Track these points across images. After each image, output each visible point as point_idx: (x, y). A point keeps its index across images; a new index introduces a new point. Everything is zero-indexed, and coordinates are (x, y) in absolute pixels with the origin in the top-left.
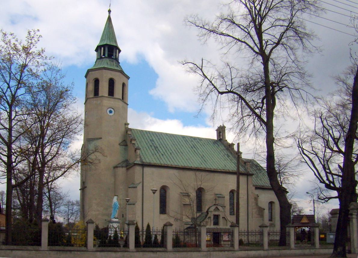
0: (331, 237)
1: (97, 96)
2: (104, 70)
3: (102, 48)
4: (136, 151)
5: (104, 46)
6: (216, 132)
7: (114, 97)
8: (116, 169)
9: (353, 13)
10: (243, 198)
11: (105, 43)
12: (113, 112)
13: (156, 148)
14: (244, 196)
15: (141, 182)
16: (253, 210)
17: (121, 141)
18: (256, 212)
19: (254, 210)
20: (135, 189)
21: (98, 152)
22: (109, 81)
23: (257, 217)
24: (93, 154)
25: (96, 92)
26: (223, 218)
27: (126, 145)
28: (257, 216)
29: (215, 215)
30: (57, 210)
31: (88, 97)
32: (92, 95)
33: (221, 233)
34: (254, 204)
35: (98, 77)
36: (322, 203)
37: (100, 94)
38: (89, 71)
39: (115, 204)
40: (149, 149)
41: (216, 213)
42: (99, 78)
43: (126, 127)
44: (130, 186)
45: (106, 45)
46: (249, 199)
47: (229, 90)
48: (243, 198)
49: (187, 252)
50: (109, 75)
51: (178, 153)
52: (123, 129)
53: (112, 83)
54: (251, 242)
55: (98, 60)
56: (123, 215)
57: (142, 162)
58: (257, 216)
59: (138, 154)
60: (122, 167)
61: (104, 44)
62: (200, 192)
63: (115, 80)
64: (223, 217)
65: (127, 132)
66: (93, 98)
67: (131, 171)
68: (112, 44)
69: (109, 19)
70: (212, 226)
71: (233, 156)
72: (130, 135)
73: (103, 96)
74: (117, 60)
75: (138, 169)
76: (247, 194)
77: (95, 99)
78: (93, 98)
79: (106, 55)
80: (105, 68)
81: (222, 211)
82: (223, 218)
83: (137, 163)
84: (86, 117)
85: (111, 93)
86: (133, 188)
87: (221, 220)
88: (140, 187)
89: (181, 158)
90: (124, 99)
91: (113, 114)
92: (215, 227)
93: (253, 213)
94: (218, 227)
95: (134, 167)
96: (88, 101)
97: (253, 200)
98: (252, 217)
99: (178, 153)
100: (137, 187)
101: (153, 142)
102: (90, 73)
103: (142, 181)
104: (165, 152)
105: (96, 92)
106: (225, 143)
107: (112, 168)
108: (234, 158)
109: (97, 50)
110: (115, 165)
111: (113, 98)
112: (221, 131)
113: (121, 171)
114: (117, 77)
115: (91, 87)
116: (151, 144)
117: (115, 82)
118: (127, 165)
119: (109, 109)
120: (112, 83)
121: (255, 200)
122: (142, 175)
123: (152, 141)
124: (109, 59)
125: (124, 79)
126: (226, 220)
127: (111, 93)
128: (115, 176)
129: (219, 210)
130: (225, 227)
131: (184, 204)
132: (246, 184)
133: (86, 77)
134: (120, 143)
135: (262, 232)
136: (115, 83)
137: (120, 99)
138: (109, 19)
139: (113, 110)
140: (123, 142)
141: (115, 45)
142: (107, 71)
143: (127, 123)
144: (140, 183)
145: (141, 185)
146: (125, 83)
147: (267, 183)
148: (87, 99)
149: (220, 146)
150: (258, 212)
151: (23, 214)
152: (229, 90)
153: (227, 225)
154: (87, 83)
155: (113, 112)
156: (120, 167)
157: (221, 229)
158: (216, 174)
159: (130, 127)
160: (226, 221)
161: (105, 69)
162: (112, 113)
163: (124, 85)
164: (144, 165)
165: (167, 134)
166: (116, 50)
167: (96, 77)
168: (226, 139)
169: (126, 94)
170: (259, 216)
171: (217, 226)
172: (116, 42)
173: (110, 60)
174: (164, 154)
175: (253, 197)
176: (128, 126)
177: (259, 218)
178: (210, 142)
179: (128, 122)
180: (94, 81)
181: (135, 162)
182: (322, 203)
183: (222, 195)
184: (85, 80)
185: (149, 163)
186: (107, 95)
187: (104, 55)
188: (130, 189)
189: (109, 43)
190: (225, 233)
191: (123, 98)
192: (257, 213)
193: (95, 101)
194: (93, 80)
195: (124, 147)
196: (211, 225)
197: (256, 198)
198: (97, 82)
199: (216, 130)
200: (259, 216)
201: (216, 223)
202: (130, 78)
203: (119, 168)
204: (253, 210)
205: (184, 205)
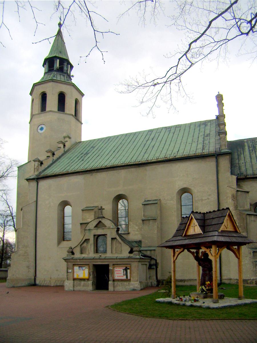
1: (45, 112)
7: (65, 112)
9: (202, 8)
10: (208, 199)
12: (43, 126)
29: (97, 237)
30: (245, 173)
31: (33, 113)
36: (226, 20)
37: (48, 109)
38: (35, 85)
41: (100, 232)
47: (186, 250)
49: (231, 168)
53: (62, 97)
54: (227, 282)
63: (66, 94)
69: (59, 33)
74: (69, 77)
76: (216, 191)
78: (39, 114)
81: (112, 227)
82: (112, 239)
90: (77, 116)
92: (97, 256)
102: (36, 87)
115: (38, 102)
119: (40, 131)
120: (62, 97)
125: (77, 95)
129: (106, 226)
133: (31, 94)
135: (24, 7)
137: (72, 115)
138: (59, 33)
141: (66, 58)
146: (78, 99)
148: (32, 116)
152: (186, 250)
163: (77, 102)
167: (42, 91)
172: (66, 53)
182: (226, 20)
184: (30, 98)
186: (56, 109)
191: (77, 114)
194: (40, 95)
198: (44, 96)
202: (84, 95)
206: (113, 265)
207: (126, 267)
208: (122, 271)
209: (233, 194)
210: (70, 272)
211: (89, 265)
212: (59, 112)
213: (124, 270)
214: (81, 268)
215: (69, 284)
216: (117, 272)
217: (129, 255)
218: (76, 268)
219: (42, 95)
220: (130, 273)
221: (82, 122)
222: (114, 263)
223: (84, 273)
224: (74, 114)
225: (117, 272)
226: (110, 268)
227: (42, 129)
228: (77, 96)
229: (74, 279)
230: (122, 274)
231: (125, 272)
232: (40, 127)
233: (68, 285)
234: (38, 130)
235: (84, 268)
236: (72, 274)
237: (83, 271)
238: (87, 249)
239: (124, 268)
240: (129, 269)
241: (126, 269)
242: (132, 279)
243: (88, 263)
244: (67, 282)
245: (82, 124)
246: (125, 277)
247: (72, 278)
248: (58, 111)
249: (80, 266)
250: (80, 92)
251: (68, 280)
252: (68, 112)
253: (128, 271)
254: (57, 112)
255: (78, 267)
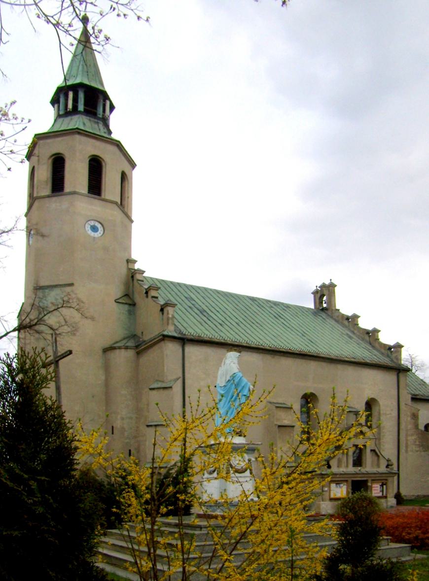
0: (310, 481)
2: (77, 137)
3: (71, 95)
4: (165, 310)
5: (75, 88)
6: (313, 296)
7: (103, 197)
8: (109, 353)
10: (391, 414)
11: (78, 81)
12: (99, 226)
13: (202, 312)
14: (392, 410)
15: (180, 378)
16: (409, 438)
17: (119, 295)
18: (416, 442)
19: (411, 439)
20: (166, 392)
21: (70, 307)
22: (90, 161)
23: (417, 451)
24: (56, 313)
25: (58, 184)
26: (371, 450)
27: (133, 305)
28: (418, 449)
32: (47, 191)
33: (366, 481)
34: (410, 427)
35: (61, 152)
37: (68, 188)
39: (236, 381)
40: (188, 313)
42: (65, 154)
43: (130, 267)
44: (152, 387)
45: (81, 85)
46: (401, 416)
48: (391, 414)
50: (87, 148)
51: (252, 325)
52: (124, 271)
53: (96, 167)
55: (61, 120)
56: (130, 451)
57: (181, 333)
58: (418, 449)
59: (170, 316)
60: (127, 348)
61: (75, 82)
62: (309, 399)
64: (373, 449)
65: (133, 277)
66: (48, 196)
67: (150, 356)
68: (93, 84)
70: (351, 469)
71: (359, 339)
72: (142, 282)
73: (74, 193)
74: (105, 122)
75: (171, 349)
76: (397, 407)
77: (54, 199)
78: (48, 196)
79: (81, 107)
80: (78, 131)
83: (170, 334)
84: (31, 242)
85: (95, 187)
86: (162, 390)
87: (368, 457)
88: (177, 387)
89: (263, 334)
91: (100, 235)
92: (357, 469)
93: (409, 443)
94: (361, 470)
95: (162, 343)
96: (36, 204)
97: (409, 419)
98: (407, 451)
99: (252, 325)
100: (173, 387)
101: (193, 302)
103: (180, 375)
104: (224, 319)
105: (58, 184)
106: (336, 314)
107: (101, 352)
108: (361, 340)
109: (55, 101)
110: (107, 346)
111: (99, 199)
112: (325, 292)
113: (123, 359)
114: (106, 153)
115: (45, 173)
116: (191, 305)
117: (103, 164)
118: (137, 344)
119: (88, 228)
120: (96, 167)
121: (412, 418)
122: (181, 361)
123: (190, 299)
124: (88, 118)
125: (126, 167)
126: (378, 456)
127: (95, 187)
128: (107, 368)
130: (375, 470)
131: (280, 425)
132: (396, 386)
134: (117, 298)
136: (104, 169)
137: (116, 203)
138: (74, 37)
139: (102, 229)
140: (123, 297)
142: (84, 139)
143: (130, 259)
144: (180, 378)
145: (180, 382)
147: (419, 390)
148: (32, 199)
149: (327, 320)
150: (419, 442)
151: (327, 559)
153: (378, 466)
154: (34, 167)
155: (99, 231)
156: (120, 348)
157: (368, 474)
158: (340, 367)
159: (137, 266)
160: (376, 458)
161: (79, 133)
162: (98, 233)
163: (124, 178)
164: (184, 341)
165: (218, 292)
166: (104, 101)
167: (58, 152)
168: (337, 308)
169: (128, 197)
170: (421, 448)
171: (359, 468)
173: (90, 120)
174: (223, 324)
175: (409, 414)
176: (134, 267)
177: (421, 452)
178: (307, 312)
179: (134, 256)
180: (50, 161)
181: (165, 333)
183: (355, 408)
185: (198, 336)
186: (85, 190)
187: (75, 107)
188: (154, 392)
189: (86, 82)
190: (373, 481)
191: (123, 204)
192: (417, 443)
193: (58, 204)
194: (49, 159)
195: (126, 307)
196: (347, 466)
197: (415, 416)
198: (58, 163)
199: (312, 293)
200: (421, 448)
201: (358, 462)
203: (117, 351)
204: (409, 438)
205: (279, 426)
206: (372, 480)
207: (383, 483)
208: (379, 486)
209: (34, 287)
210: (326, 491)
211: (347, 481)
212: (90, 195)
213: (380, 486)
214: (338, 485)
215: (327, 506)
216: (375, 489)
217: (386, 469)
218: (333, 486)
219: (53, 159)
220: (386, 489)
221: (133, 218)
222: (373, 478)
223: (342, 491)
224: (119, 203)
225: (375, 489)
226: (369, 484)
227: (94, 229)
228: (126, 167)
229: (331, 499)
230: (379, 491)
231: (381, 489)
232: (92, 223)
233: (325, 507)
234: (87, 225)
235: (342, 485)
236: (328, 493)
237: (340, 489)
238: (343, 462)
239: (381, 484)
240: (385, 484)
241: (382, 486)
242: (388, 496)
243: (346, 479)
244: (324, 504)
245: (132, 221)
246: (380, 494)
247: (328, 498)
248: (89, 193)
249: (338, 483)
250: (129, 158)
251: (323, 501)
252: (107, 197)
253: (385, 486)
254: (51, 197)
255: (335, 484)
